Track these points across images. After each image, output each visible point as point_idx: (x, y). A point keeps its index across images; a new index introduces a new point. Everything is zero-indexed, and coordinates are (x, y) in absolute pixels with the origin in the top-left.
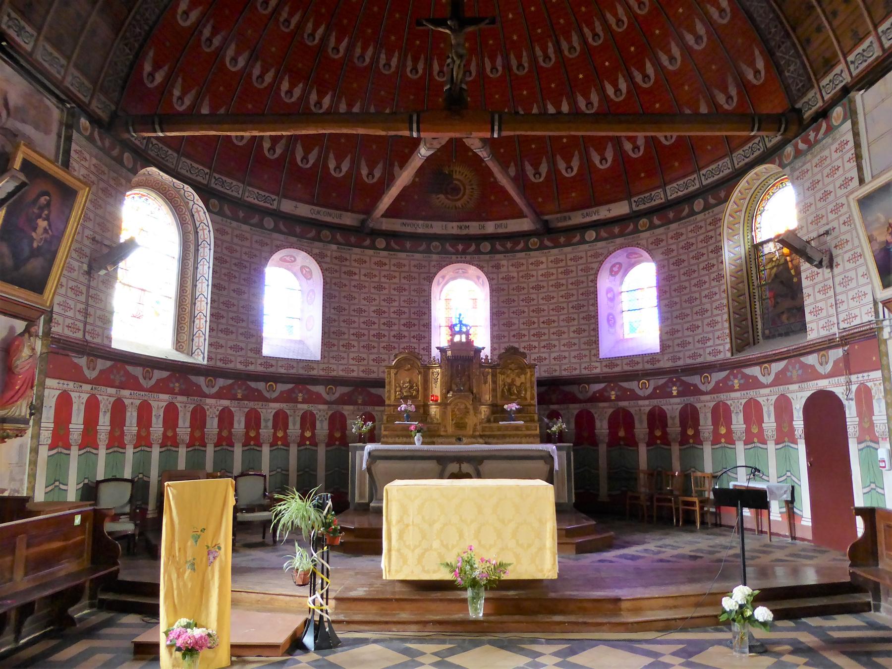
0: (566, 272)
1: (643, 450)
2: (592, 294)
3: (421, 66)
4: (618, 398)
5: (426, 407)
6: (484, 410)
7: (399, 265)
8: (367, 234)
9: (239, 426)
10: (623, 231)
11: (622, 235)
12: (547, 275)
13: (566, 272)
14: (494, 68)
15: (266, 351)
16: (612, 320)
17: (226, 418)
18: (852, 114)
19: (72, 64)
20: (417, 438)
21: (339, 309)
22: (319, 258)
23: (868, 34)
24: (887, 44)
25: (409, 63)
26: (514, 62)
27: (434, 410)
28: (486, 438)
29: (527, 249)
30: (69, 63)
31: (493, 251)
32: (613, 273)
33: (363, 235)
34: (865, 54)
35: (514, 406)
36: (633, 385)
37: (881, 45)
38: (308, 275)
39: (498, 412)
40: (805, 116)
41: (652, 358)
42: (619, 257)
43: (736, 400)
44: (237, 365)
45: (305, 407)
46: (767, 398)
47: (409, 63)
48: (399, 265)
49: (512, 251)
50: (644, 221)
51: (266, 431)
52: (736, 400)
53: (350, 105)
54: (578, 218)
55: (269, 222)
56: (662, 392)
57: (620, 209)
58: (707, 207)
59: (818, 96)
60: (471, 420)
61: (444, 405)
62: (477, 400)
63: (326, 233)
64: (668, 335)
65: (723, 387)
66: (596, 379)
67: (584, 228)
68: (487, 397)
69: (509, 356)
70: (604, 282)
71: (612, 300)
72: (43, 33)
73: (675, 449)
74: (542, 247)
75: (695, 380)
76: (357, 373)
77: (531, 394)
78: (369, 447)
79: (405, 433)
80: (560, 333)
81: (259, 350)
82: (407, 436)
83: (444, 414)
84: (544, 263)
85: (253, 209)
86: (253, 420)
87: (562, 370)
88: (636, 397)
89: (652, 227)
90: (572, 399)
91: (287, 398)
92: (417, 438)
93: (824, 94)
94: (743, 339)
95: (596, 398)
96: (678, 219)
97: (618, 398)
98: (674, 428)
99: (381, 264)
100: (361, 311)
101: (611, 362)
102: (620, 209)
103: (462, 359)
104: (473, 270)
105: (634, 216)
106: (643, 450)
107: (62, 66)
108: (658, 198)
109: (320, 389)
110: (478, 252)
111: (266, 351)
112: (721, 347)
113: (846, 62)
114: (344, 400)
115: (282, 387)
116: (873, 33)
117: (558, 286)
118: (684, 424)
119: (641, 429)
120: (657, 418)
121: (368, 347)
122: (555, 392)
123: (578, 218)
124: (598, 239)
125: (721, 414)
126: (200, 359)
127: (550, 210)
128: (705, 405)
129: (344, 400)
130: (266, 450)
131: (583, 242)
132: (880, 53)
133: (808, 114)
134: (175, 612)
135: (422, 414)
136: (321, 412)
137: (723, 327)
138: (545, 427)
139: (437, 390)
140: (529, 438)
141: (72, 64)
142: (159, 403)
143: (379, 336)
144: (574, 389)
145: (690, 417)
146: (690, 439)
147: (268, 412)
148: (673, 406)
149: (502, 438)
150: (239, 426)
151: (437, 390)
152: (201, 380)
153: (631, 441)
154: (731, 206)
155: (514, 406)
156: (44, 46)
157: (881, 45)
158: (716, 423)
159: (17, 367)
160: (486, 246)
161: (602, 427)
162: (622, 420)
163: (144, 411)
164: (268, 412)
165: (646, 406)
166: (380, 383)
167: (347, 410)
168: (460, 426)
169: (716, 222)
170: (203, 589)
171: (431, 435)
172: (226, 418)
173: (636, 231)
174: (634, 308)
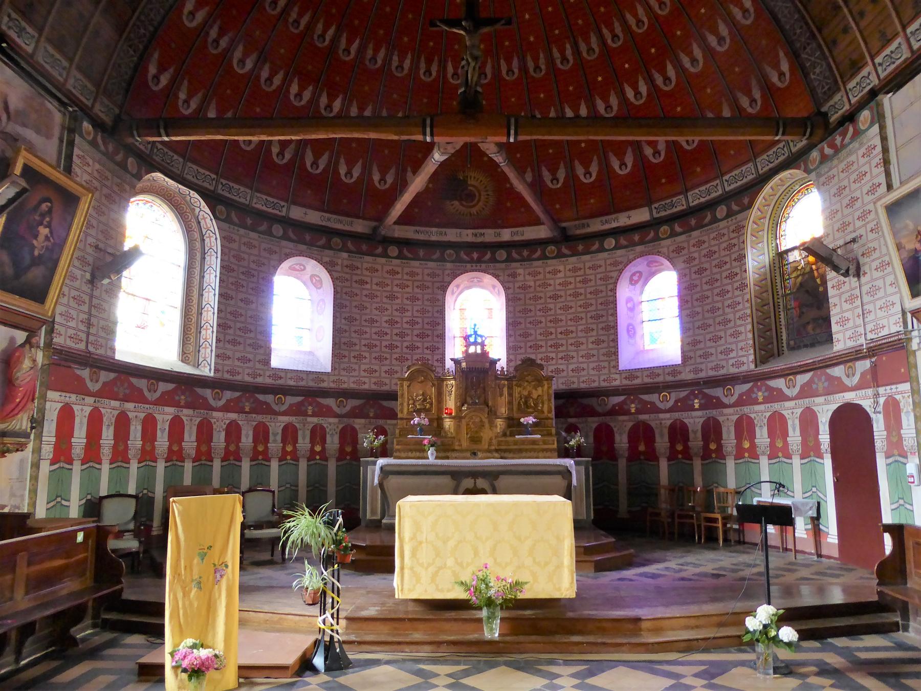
0: (585, 281)
1: (664, 464)
2: (611, 304)
3: (434, 69)
4: (638, 412)
5: (440, 420)
6: (500, 423)
7: (412, 274)
8: (379, 242)
9: (247, 440)
10: (643, 239)
11: (642, 242)
12: (565, 284)
13: (585, 281)
14: (510, 70)
15: (275, 363)
16: (632, 331)
17: (233, 432)
18: (879, 118)
19: (74, 66)
20: (431, 452)
21: (351, 320)
22: (329, 267)
23: (896, 35)
24: (916, 46)
25: (423, 66)
26: (531, 64)
27: (448, 423)
28: (502, 452)
29: (544, 257)
30: (71, 65)
31: (509, 259)
32: (633, 282)
33: (375, 243)
34: (893, 55)
35: (531, 420)
36: (653, 398)
37: (910, 46)
38: (318, 284)
39: (514, 425)
40: (832, 120)
41: (673, 369)
42: (639, 265)
43: (760, 413)
44: (245, 377)
45: (315, 420)
46: (792, 412)
47: (423, 66)
48: (412, 274)
49: (529, 259)
50: (665, 228)
51: (275, 445)
52: (760, 413)
53: (361, 109)
54: (596, 225)
55: (278, 230)
56: (684, 405)
57: (641, 215)
58: (730, 214)
59: (845, 99)
60: (487, 434)
61: (458, 418)
62: (493, 413)
63: (336, 240)
64: (690, 346)
65: (746, 400)
66: (616, 392)
67: (603, 235)
68: (503, 410)
69: (526, 368)
70: (624, 291)
71: (632, 310)
72: (45, 34)
73: (697, 464)
74: (560, 255)
75: (718, 392)
76: (369, 385)
77: (548, 407)
78: (381, 462)
79: (418, 447)
80: (578, 344)
81: (267, 362)
82: (420, 450)
83: (458, 428)
84: (561, 271)
85: (261, 216)
86: (261, 434)
87: (580, 383)
88: (656, 410)
89: (673, 234)
90: (591, 412)
91: (296, 411)
92: (431, 452)
93: (851, 97)
94: (767, 350)
95: (615, 412)
96: (700, 226)
97: (638, 412)
98: (696, 442)
99: (393, 273)
100: (373, 321)
101: (631, 374)
102: (641, 215)
103: (477, 370)
104: (488, 279)
105: (655, 224)
106: (664, 464)
107: (64, 68)
108: (680, 204)
109: (330, 402)
110: (493, 260)
111: (275, 363)
112: (744, 359)
113: (874, 64)
114: (355, 413)
115: (291, 400)
116: (902, 34)
117: (576, 295)
118: (706, 438)
119: (662, 443)
120: (678, 432)
121: (380, 359)
122: (573, 405)
123: (596, 225)
124: (617, 247)
125: (745, 428)
126: (207, 371)
127: (568, 217)
128: (728, 419)
129: (355, 413)
130: (274, 465)
131: (602, 249)
132: (909, 55)
133: (834, 118)
134: (181, 633)
135: (436, 427)
136: (332, 425)
137: (747, 338)
138: (563, 441)
139: (451, 403)
140: (546, 453)
141: (74, 66)
142: (164, 416)
143: (391, 347)
144: (593, 402)
145: (712, 430)
146: (712, 453)
147: (276, 425)
148: (695, 420)
149: (519, 452)
150: (247, 440)
151: (451, 403)
152: (208, 393)
153: (652, 456)
154: (754, 213)
155: (531, 420)
156: (45, 48)
157: (910, 46)
158: (739, 436)
159: (17, 379)
160: (502, 254)
161: (622, 441)
162: (643, 434)
163: (149, 425)
164: (276, 425)
165: (667, 419)
166: (393, 396)
167: (358, 423)
168: (475, 440)
169: (740, 229)
170: (210, 608)
171: (445, 449)
172: (233, 432)
173: (657, 238)
174: (654, 318)
